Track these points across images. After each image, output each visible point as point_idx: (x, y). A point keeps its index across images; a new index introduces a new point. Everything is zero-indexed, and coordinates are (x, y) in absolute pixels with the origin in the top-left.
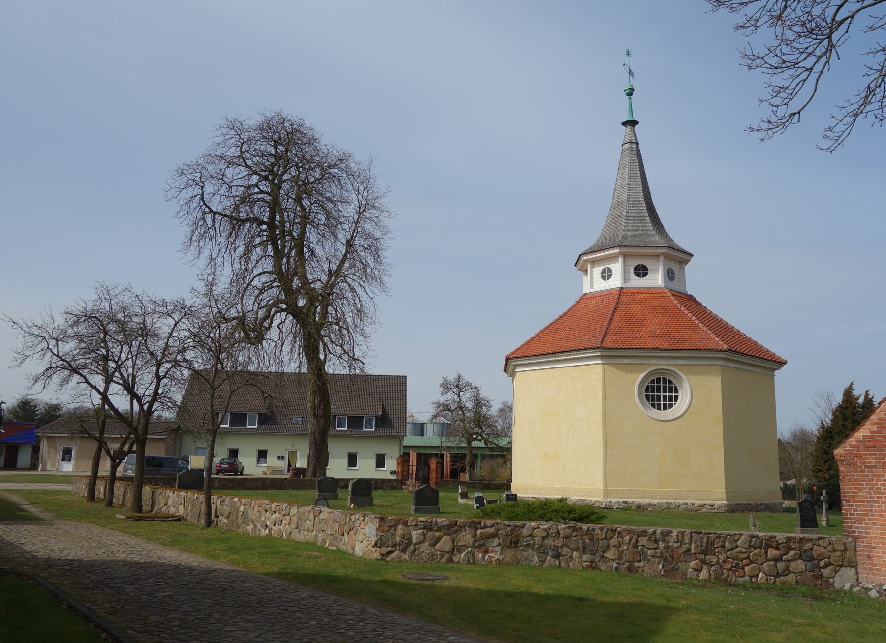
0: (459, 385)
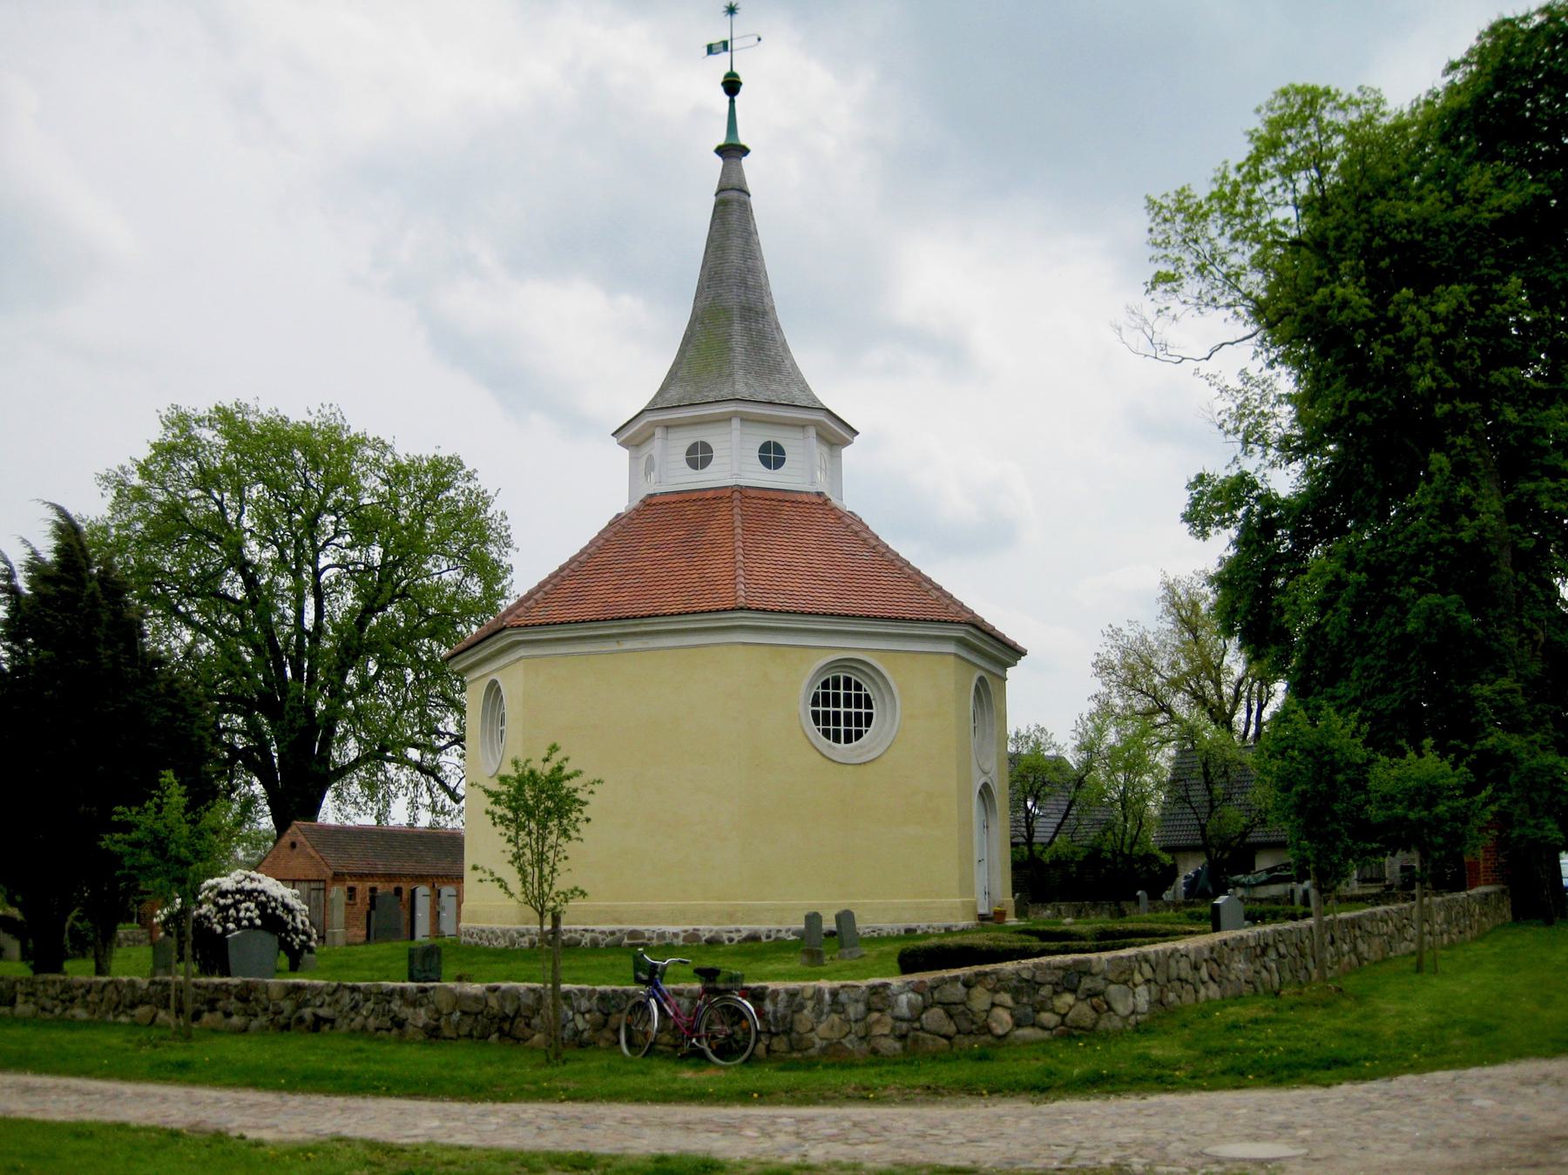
0: (1043, 730)
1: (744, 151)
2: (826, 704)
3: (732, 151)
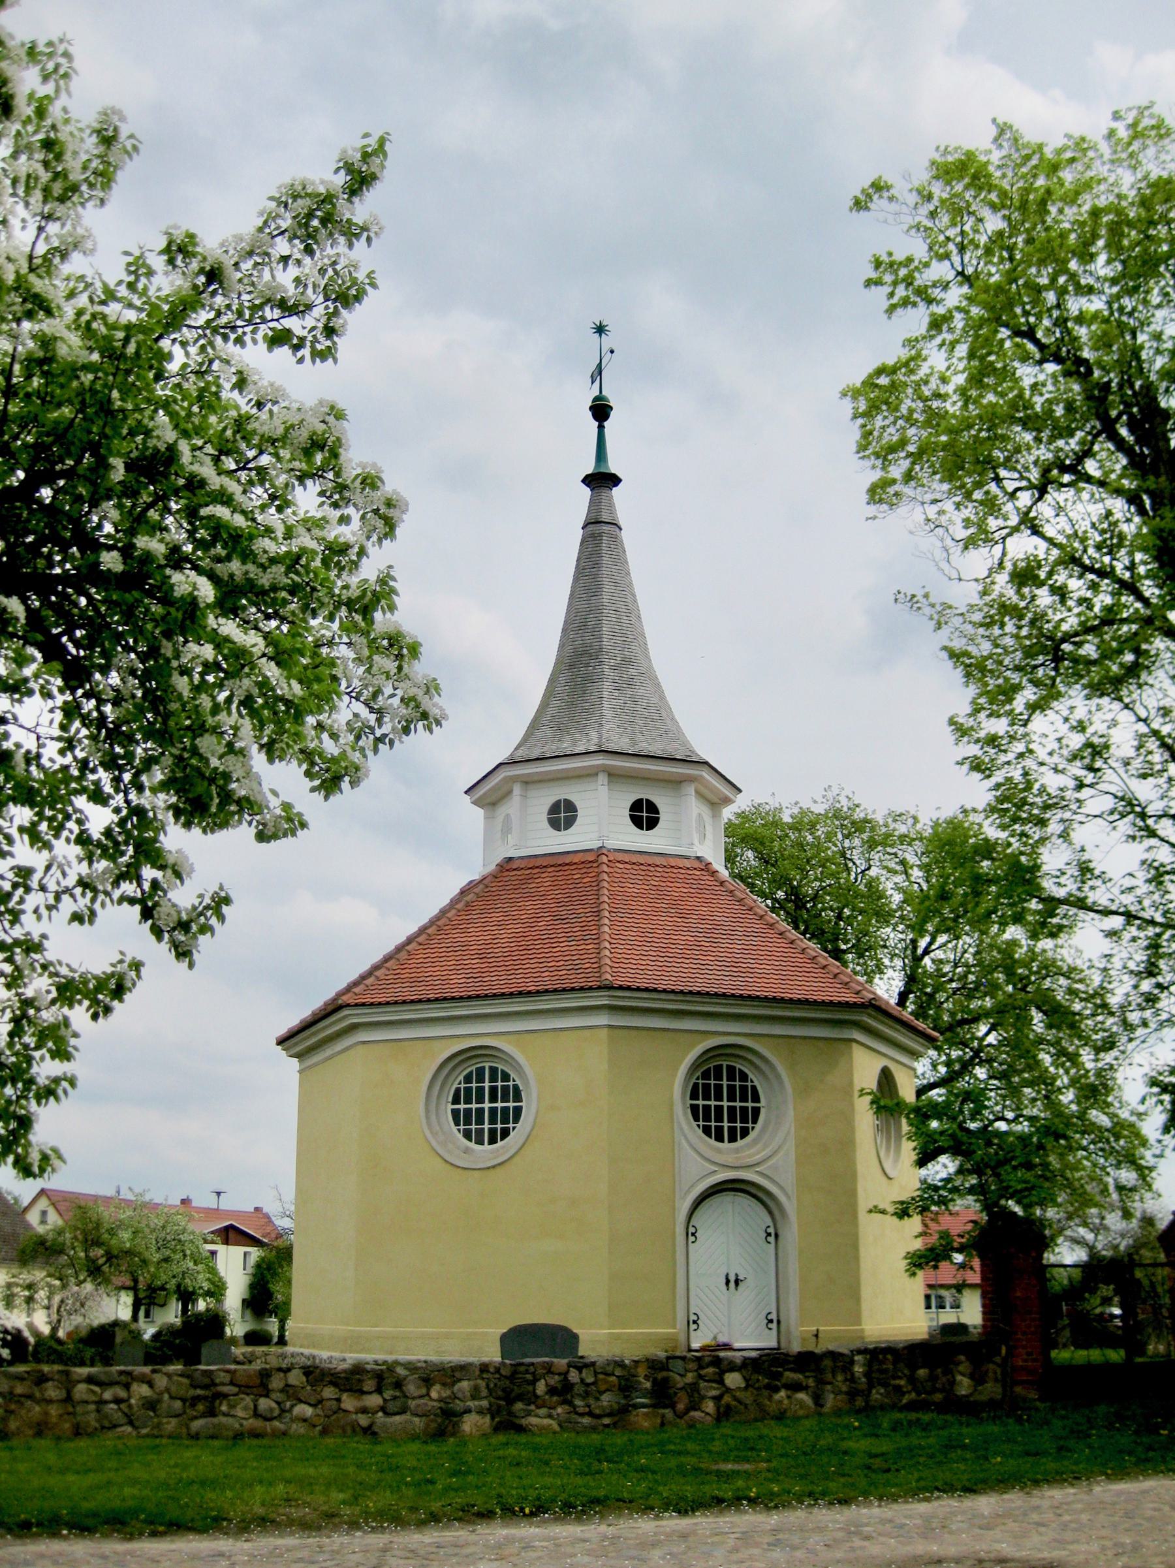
1: (614, 480)
2: (744, 1110)
3: (601, 480)
